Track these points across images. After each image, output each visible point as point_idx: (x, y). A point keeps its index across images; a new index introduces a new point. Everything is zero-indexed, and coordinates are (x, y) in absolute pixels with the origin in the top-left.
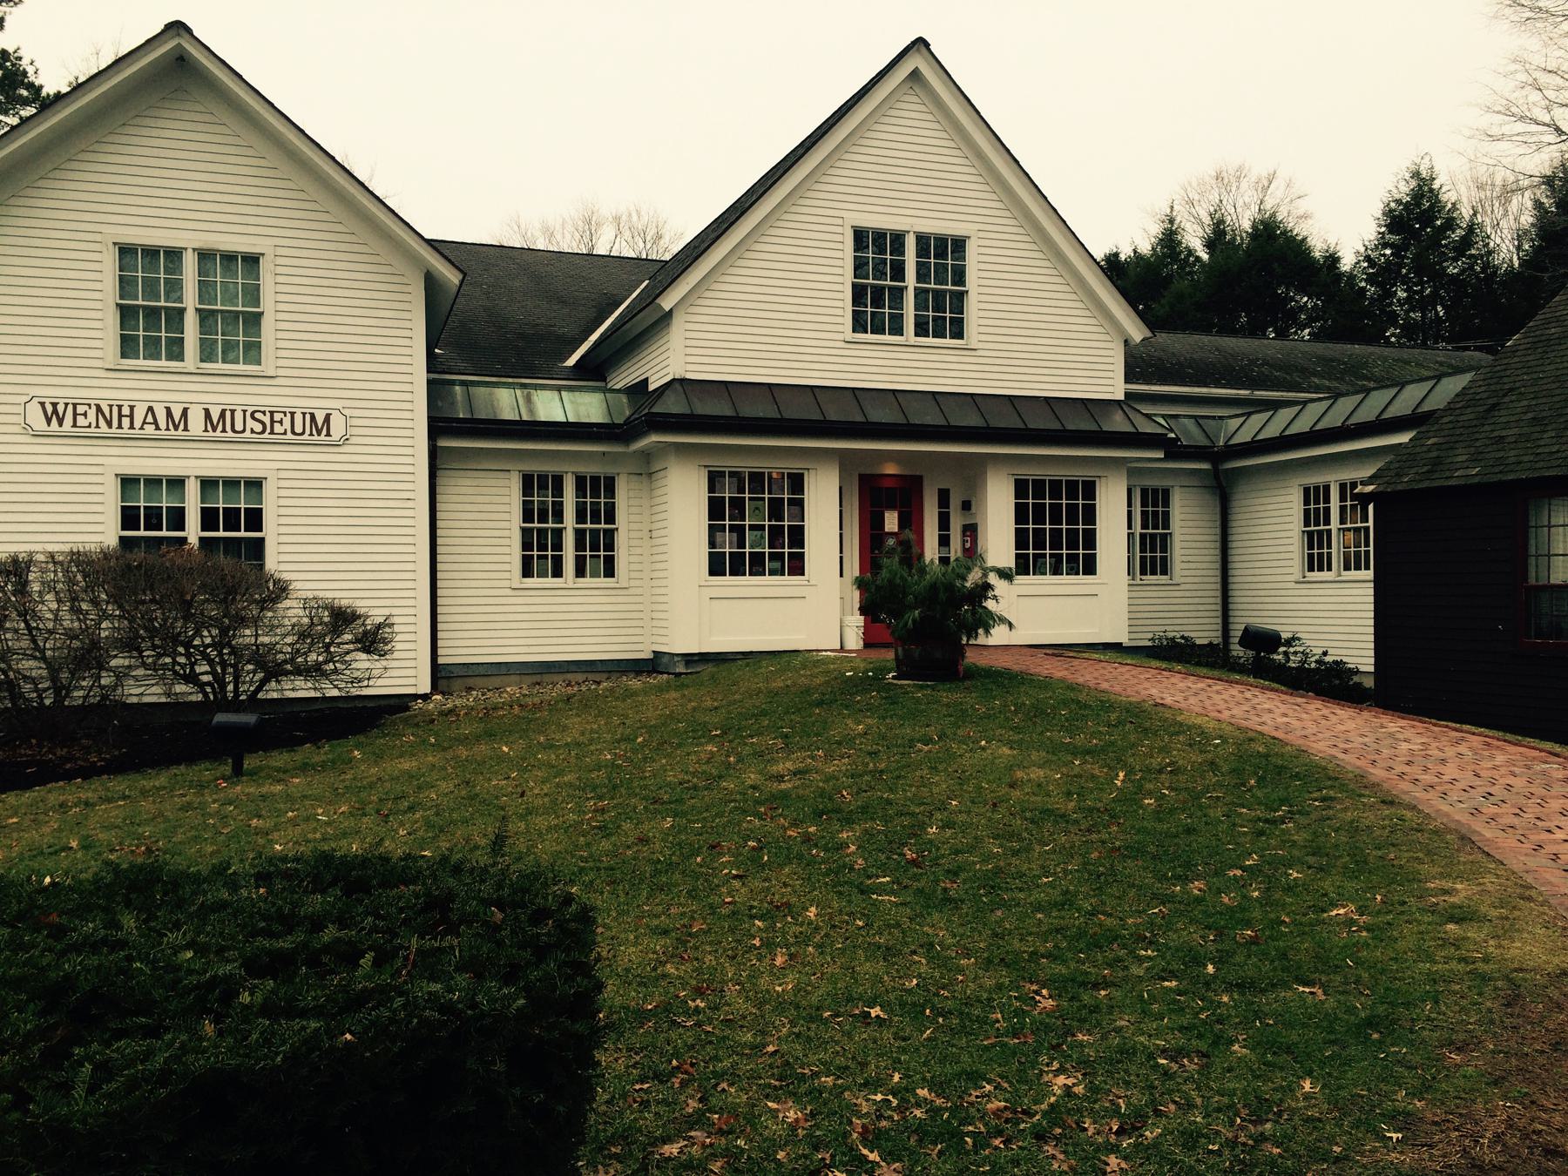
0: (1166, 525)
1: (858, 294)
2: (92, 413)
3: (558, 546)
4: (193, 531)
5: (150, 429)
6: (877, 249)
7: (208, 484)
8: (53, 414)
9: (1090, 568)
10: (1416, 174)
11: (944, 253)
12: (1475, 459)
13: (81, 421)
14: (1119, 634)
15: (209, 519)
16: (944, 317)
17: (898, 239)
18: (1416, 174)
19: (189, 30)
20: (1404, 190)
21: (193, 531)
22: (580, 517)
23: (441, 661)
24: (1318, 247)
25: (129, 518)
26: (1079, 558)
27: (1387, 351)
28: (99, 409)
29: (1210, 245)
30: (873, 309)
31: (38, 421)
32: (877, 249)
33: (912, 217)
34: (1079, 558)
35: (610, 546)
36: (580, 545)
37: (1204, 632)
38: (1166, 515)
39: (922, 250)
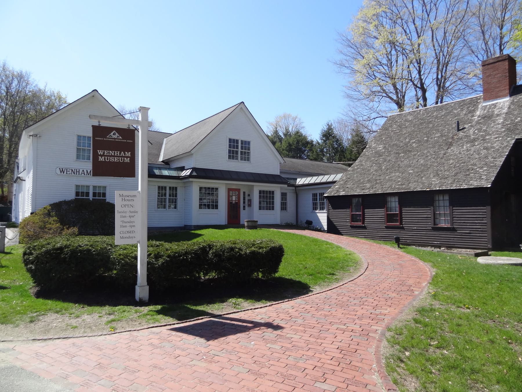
0: (286, 200)
1: (230, 151)
2: (70, 171)
3: (165, 202)
4: (91, 197)
5: (83, 175)
6: (233, 143)
7: (94, 187)
8: (62, 171)
9: (273, 209)
10: (328, 125)
11: (246, 145)
12: (344, 191)
13: (68, 173)
14: (278, 222)
15: (94, 194)
16: (246, 156)
17: (237, 141)
18: (328, 125)
19: (97, 91)
20: (326, 128)
21: (91, 197)
22: (170, 196)
23: (389, 199)
24: (309, 139)
25: (77, 194)
26: (270, 207)
27: (323, 163)
28: (72, 170)
29: (285, 135)
30: (232, 155)
31: (59, 172)
32: (233, 143)
33: (240, 137)
34: (270, 207)
35: (176, 202)
36: (169, 202)
37: (293, 221)
38: (286, 198)
39: (242, 143)
